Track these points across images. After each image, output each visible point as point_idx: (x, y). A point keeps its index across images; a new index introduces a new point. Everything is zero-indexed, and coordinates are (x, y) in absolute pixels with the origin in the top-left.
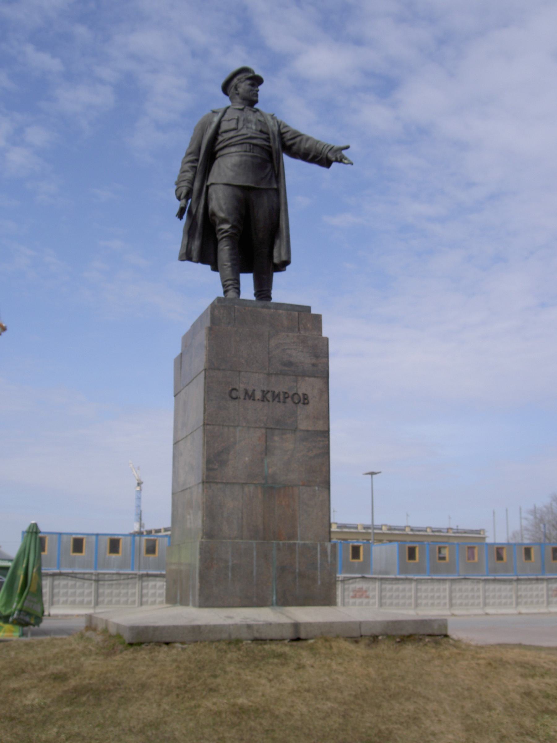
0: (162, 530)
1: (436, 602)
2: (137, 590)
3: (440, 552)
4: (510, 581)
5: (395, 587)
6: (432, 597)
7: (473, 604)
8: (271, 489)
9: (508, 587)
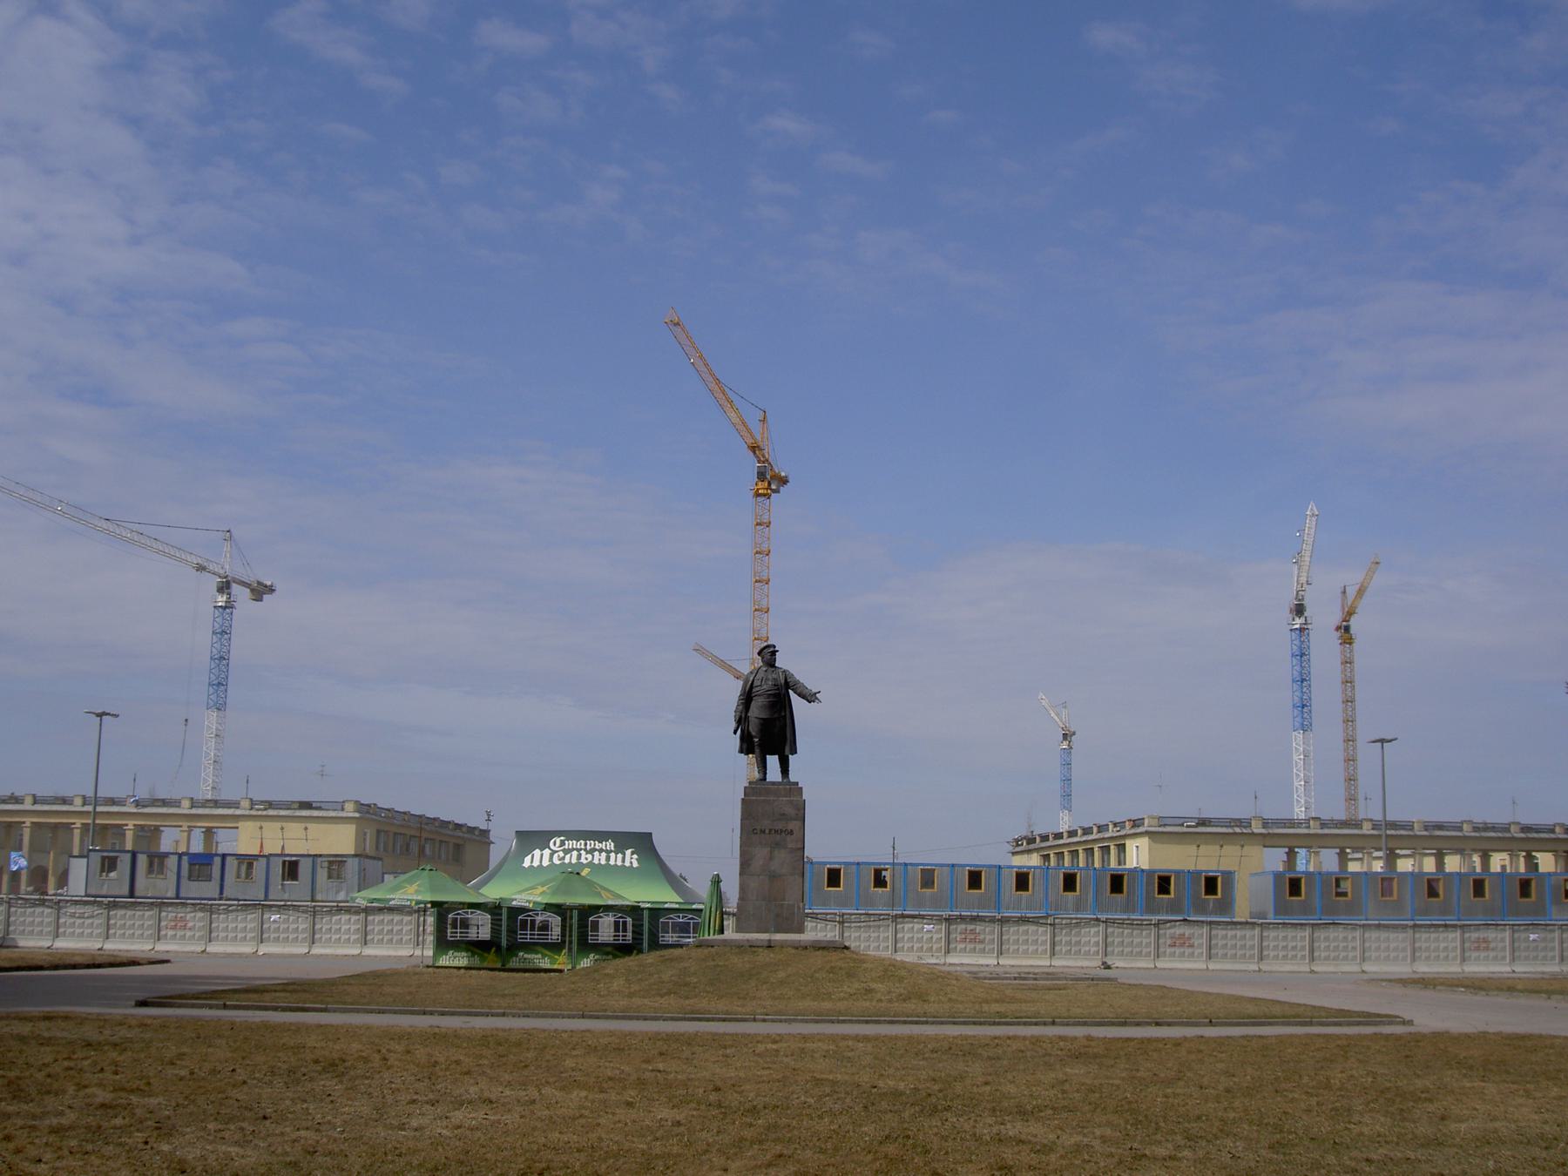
1: (1291, 954)
2: (890, 934)
3: (1338, 885)
5: (1230, 933)
6: (1285, 948)
7: (1346, 958)
8: (773, 877)
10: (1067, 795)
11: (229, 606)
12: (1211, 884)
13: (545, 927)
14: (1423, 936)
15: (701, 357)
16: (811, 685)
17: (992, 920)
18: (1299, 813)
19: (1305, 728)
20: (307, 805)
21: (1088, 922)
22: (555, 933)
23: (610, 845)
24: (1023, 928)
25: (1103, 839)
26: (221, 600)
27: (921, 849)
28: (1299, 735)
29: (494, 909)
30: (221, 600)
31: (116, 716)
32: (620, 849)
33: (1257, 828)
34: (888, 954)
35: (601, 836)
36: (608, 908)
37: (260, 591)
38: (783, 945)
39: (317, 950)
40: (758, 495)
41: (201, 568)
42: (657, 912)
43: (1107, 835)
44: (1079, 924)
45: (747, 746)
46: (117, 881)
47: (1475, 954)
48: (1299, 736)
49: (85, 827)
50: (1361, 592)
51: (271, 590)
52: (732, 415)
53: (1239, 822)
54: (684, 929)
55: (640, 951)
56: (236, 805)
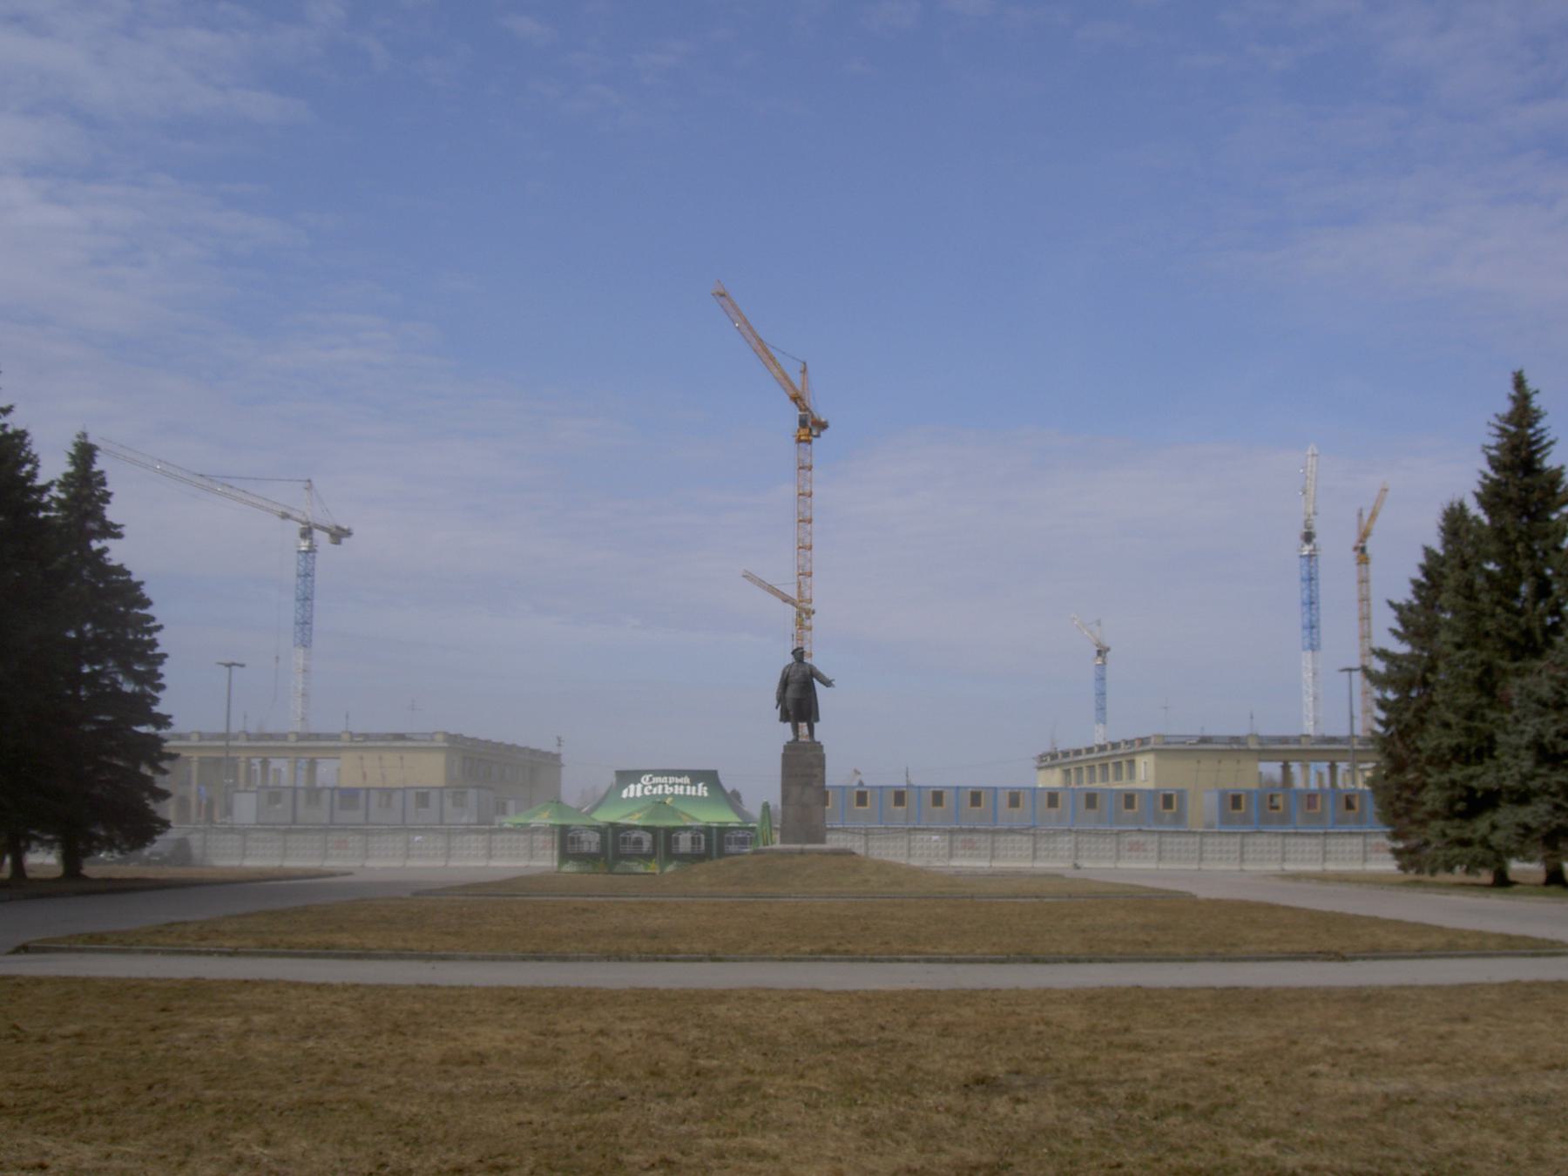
0: (292, 738)
2: (1030, 845)
4: (1317, 835)
5: (1177, 840)
9: (1314, 841)
10: (1101, 709)
12: (1168, 801)
13: (639, 842)
14: (1332, 841)
15: (745, 322)
16: (828, 675)
18: (1309, 728)
19: (1313, 647)
20: (401, 737)
21: (1063, 832)
22: (646, 846)
23: (686, 780)
24: (1010, 838)
26: (304, 545)
27: (929, 777)
28: (1309, 654)
29: (602, 830)
30: (304, 545)
31: (242, 666)
32: (694, 783)
33: (1253, 746)
34: (903, 861)
36: (686, 829)
37: (339, 535)
38: (811, 852)
40: (799, 441)
41: (285, 516)
42: (723, 830)
44: (1056, 833)
45: (785, 717)
47: (1374, 856)
48: (1307, 656)
50: (1373, 516)
51: (348, 533)
53: (1235, 740)
54: (743, 842)
56: (336, 737)
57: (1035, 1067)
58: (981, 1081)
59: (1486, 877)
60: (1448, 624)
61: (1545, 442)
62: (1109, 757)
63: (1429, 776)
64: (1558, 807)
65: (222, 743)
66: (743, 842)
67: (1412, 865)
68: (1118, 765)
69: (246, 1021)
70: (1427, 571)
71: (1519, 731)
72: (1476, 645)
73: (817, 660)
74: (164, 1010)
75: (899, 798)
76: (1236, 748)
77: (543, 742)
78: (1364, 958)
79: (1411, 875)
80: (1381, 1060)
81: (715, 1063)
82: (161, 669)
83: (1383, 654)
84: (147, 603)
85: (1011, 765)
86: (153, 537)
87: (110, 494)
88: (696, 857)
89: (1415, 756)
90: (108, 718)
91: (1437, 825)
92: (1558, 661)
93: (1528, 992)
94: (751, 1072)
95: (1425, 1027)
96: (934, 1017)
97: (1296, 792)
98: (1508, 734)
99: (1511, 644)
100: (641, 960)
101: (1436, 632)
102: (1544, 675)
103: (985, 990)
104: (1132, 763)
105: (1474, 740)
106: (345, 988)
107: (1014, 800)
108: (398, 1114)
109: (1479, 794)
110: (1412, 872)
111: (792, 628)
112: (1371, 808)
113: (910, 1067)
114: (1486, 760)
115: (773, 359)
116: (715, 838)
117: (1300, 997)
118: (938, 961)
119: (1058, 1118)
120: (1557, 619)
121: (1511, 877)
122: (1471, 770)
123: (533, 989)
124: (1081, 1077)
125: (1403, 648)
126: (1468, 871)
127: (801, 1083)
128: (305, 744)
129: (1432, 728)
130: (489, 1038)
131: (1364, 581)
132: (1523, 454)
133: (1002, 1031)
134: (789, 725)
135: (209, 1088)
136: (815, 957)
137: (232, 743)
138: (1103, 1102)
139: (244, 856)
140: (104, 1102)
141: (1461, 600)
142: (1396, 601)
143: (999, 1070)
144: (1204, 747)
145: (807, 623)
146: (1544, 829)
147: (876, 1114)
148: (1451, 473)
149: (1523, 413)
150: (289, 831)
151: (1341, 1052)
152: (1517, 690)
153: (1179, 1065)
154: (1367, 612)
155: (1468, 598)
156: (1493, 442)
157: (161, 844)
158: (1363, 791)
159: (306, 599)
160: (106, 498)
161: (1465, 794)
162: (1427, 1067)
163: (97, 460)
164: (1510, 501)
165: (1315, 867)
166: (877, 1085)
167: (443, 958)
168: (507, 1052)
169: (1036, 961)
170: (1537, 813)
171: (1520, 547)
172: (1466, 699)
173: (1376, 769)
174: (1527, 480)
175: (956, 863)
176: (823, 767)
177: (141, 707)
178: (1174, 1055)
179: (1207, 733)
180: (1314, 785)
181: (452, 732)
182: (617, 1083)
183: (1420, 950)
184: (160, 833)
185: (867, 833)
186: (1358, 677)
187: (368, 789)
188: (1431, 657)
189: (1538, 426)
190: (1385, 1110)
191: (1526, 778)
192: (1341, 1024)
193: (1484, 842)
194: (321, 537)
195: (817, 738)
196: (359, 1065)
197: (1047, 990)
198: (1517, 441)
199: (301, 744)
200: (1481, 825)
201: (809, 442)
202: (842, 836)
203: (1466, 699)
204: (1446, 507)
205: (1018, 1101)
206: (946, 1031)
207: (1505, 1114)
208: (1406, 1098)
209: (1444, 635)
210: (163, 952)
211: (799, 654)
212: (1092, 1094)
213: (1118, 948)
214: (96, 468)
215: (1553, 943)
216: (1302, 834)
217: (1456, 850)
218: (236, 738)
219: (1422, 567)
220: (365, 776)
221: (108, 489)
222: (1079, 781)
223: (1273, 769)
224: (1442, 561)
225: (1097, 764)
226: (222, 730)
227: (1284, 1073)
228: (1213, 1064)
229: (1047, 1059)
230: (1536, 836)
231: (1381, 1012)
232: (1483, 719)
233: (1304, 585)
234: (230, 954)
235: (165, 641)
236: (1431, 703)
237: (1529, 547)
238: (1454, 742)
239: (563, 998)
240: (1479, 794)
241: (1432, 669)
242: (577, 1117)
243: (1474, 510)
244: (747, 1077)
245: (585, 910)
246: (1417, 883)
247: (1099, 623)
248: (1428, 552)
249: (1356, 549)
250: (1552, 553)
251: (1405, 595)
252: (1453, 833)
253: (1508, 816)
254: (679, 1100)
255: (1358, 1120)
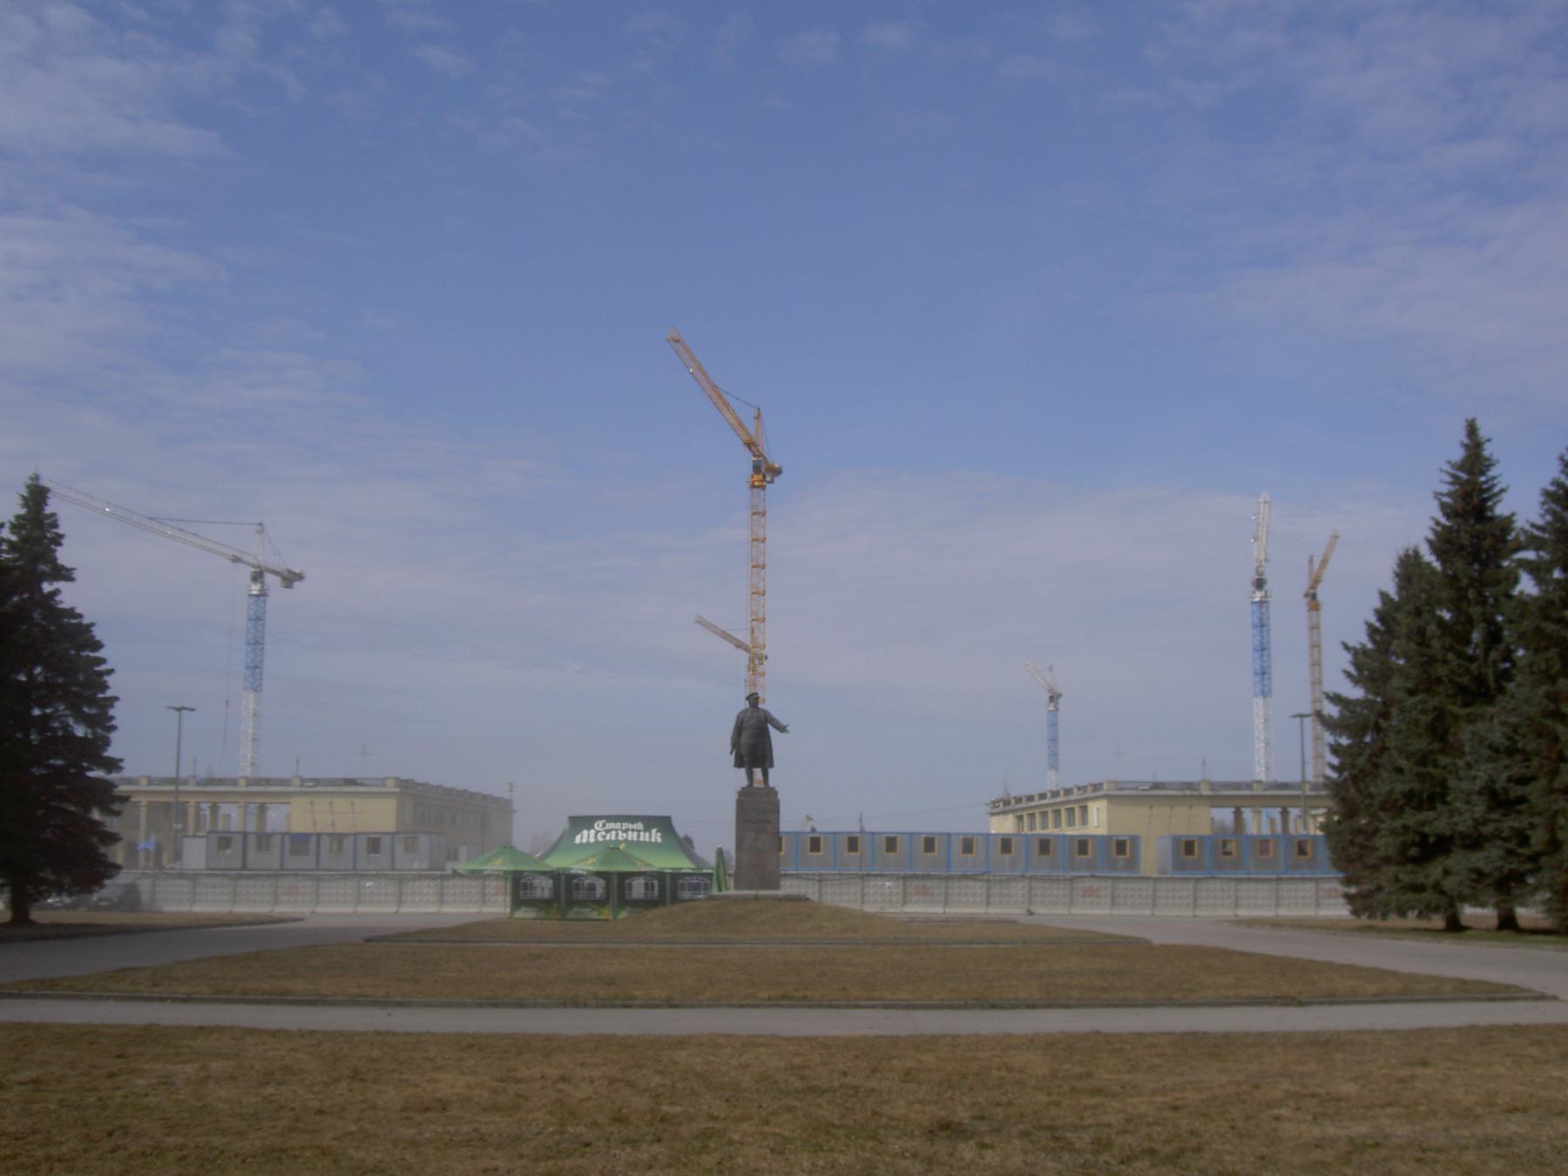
0: (242, 782)
4: (1269, 880)
9: (1266, 887)
10: (1054, 755)
11: (263, 594)
12: (1121, 846)
13: (592, 888)
14: (1285, 886)
15: (700, 368)
16: (783, 721)
17: (940, 878)
18: (1260, 774)
19: (1265, 693)
21: (1016, 878)
22: (599, 892)
23: (640, 826)
24: (964, 883)
25: (1068, 802)
26: (255, 589)
27: (883, 822)
28: (1260, 700)
29: (555, 876)
30: (255, 589)
32: (647, 829)
33: (1205, 791)
34: (856, 906)
35: (632, 819)
37: (290, 579)
38: (765, 898)
39: (404, 910)
40: (753, 487)
41: (236, 560)
42: (676, 876)
43: (1072, 797)
44: (1009, 880)
45: (739, 763)
46: (231, 856)
49: (151, 805)
50: (1324, 562)
51: (300, 577)
52: (729, 416)
53: (1190, 786)
54: (696, 888)
55: (664, 904)
56: (286, 782)
57: (1000, 1112)
58: (945, 1126)
59: (1438, 921)
60: (1400, 670)
61: (1496, 490)
62: (1062, 803)
63: (1382, 821)
64: (1510, 852)
65: (172, 788)
66: (696, 888)
67: (1365, 909)
68: (1071, 811)
69: (203, 1068)
70: (1382, 615)
71: (1472, 776)
72: (1427, 691)
73: (769, 705)
74: (119, 1057)
75: (853, 843)
76: (1188, 794)
77: (496, 789)
78: (1321, 1003)
79: (1364, 920)
80: (1343, 1104)
81: (678, 1109)
82: (111, 712)
83: (1336, 699)
84: (98, 646)
85: (962, 808)
86: (98, 581)
87: (61, 536)
88: (648, 903)
89: (1368, 801)
90: (59, 762)
91: (1390, 870)
92: (1509, 707)
93: (1486, 1036)
94: (715, 1118)
95: (1385, 1071)
96: (895, 1062)
97: (1252, 838)
98: (1460, 779)
99: (1462, 689)
100: (597, 1006)
101: (1389, 678)
102: (1496, 721)
103: (945, 1036)
104: (1084, 809)
105: (1427, 785)
106: (303, 1034)
107: (968, 846)
108: (363, 1161)
109: (1432, 840)
110: (1364, 917)
111: (744, 673)
112: (1324, 853)
113: (875, 1113)
114: (1439, 806)
115: (727, 405)
116: (668, 885)
117: (1260, 1041)
118: (896, 1007)
119: (1025, 1162)
120: (1507, 665)
121: (1464, 922)
122: (1423, 816)
123: (491, 1035)
124: (1045, 1122)
125: (1356, 693)
126: (1420, 915)
127: (766, 1129)
128: (256, 789)
129: (1384, 774)
130: (450, 1084)
131: (1315, 628)
132: (1476, 500)
133: (964, 1076)
134: (743, 771)
135: (169, 1134)
136: (772, 1003)
137: (181, 788)
138: (1070, 1147)
139: (194, 902)
140: (64, 1149)
141: (1413, 645)
142: (1351, 644)
143: (963, 1115)
144: (1156, 794)
145: (760, 669)
146: (1497, 874)
147: (842, 1159)
148: (1385, 528)
149: (1475, 460)
150: (239, 877)
151: (1305, 1096)
152: (1468, 736)
153: (1143, 1109)
154: (1323, 655)
155: (1420, 644)
156: (1445, 489)
157: (112, 888)
158: (1316, 837)
159: (257, 643)
160: (58, 540)
161: (1417, 839)
162: (1389, 1110)
163: (49, 502)
164: (1462, 548)
165: (1268, 913)
166: (841, 1132)
167: (399, 1005)
168: (469, 1099)
169: (993, 1007)
170: (1490, 858)
171: (1471, 594)
172: (1419, 745)
173: (1329, 814)
174: (1479, 527)
175: (909, 909)
176: (777, 812)
177: (94, 750)
178: (1137, 1100)
179: (1161, 779)
180: (1266, 831)
181: (404, 776)
182: (581, 1129)
183: (1375, 995)
184: (110, 877)
185: (821, 880)
186: (1308, 722)
187: (319, 835)
188: (1385, 703)
189: (1491, 474)
190: (1350, 1153)
191: (1478, 823)
192: (1301, 1068)
193: (1437, 887)
194: (272, 581)
195: (772, 783)
196: (320, 1112)
197: (1007, 1036)
198: (1469, 488)
199: (251, 789)
200: (1434, 871)
201: (763, 488)
202: (795, 883)
203: (1419, 745)
204: (1401, 553)
205: (983, 1146)
206: (908, 1076)
207: (1469, 1157)
208: (1370, 1142)
209: (1396, 682)
210: (116, 999)
211: (753, 699)
212: (1057, 1139)
213: (1076, 994)
214: (48, 510)
215: (1508, 987)
216: (1256, 880)
217: (1410, 896)
218: (185, 782)
219: (1377, 611)
220: (315, 822)
221: (60, 531)
222: (1032, 827)
223: (1225, 815)
224: (1397, 607)
225: (1049, 810)
226: (173, 775)
227: (1248, 1118)
228: (1176, 1108)
229: (1010, 1104)
230: (1490, 881)
231: (1340, 1056)
232: (1436, 766)
233: (1256, 631)
234: (183, 1001)
235: (115, 685)
236: (1384, 749)
237: (1480, 594)
238: (1407, 787)
239: (522, 1045)
240: (1432, 840)
241: (1385, 715)
242: (542, 1164)
243: (1428, 556)
244: (711, 1124)
245: (539, 957)
246: (1371, 928)
247: (1051, 669)
248: (1384, 596)
249: (1306, 595)
250: (1502, 599)
251: (1360, 638)
252: (1406, 878)
253: (1460, 862)
254: (644, 1146)
255: (1323, 1163)
